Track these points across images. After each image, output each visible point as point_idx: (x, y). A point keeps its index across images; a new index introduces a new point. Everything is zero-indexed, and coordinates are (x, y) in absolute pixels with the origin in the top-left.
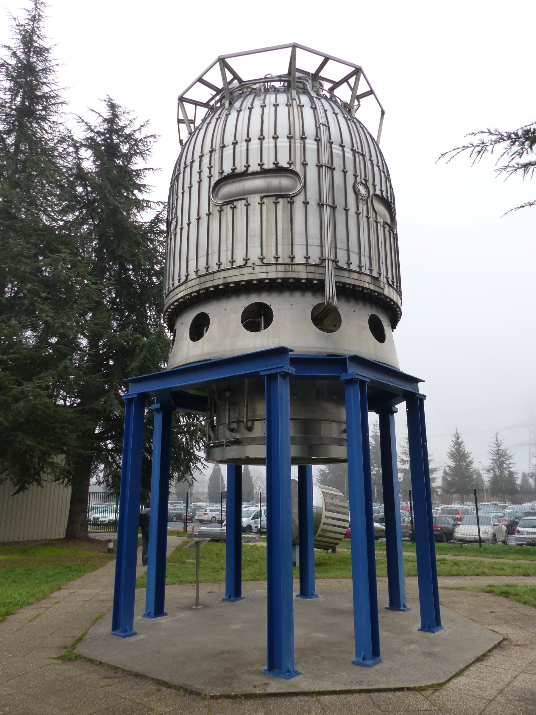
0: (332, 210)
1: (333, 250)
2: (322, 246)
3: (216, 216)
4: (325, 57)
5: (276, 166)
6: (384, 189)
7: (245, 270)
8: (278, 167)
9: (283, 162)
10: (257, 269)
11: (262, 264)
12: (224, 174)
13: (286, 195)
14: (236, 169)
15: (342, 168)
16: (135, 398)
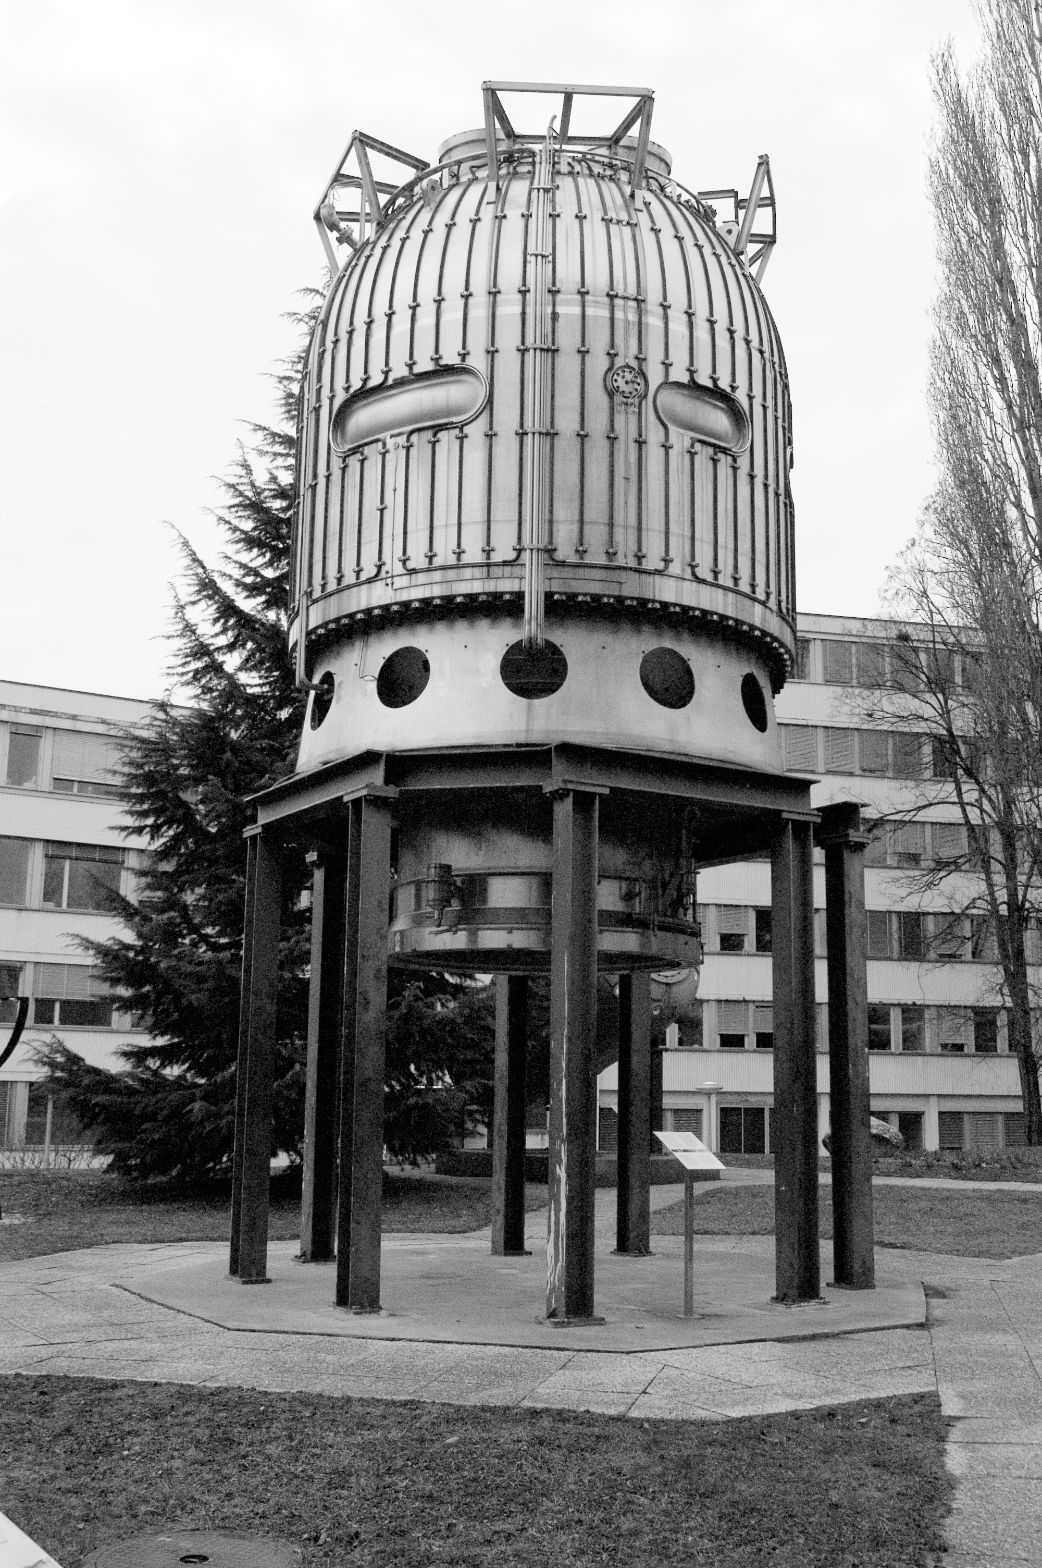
5: (437, 364)
7: (379, 586)
9: (450, 357)
10: (399, 582)
12: (352, 391)
13: (452, 423)
15: (684, 306)
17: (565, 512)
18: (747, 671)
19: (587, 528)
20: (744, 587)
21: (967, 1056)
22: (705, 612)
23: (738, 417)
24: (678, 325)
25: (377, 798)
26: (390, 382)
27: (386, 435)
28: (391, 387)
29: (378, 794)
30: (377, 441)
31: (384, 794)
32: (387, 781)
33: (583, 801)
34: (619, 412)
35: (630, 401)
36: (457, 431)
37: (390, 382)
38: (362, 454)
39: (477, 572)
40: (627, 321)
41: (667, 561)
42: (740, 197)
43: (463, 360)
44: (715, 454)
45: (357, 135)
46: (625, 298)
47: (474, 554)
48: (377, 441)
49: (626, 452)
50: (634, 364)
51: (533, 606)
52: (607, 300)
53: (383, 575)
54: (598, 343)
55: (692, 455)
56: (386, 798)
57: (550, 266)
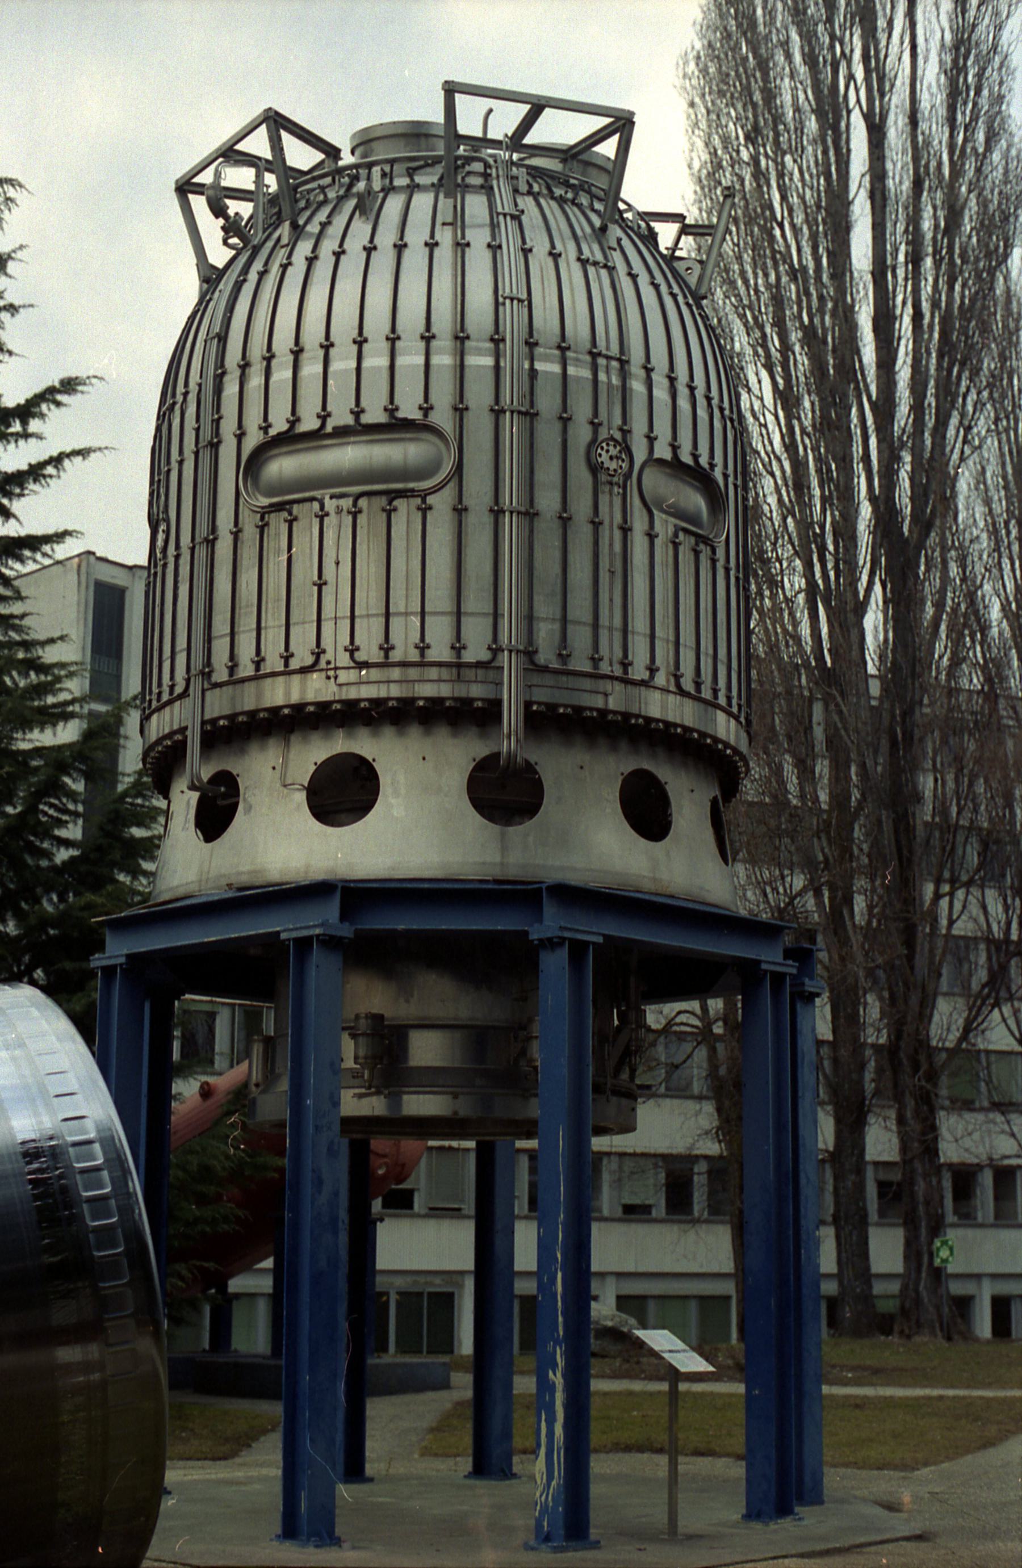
0: (525, 521)
1: (524, 624)
2: (496, 616)
3: (250, 532)
4: (533, 104)
6: (718, 459)
8: (396, 419)
9: (409, 409)
11: (352, 664)
12: (273, 432)
13: (413, 490)
14: (298, 420)
16: (121, 965)
17: (545, 608)
18: (629, 764)
19: (570, 628)
20: (706, 694)
21: (656, 1221)
22: (667, 724)
23: (716, 499)
24: (661, 393)
25: (332, 937)
26: (329, 429)
27: (325, 493)
28: (329, 436)
29: (333, 933)
30: (312, 499)
31: (339, 934)
32: (344, 917)
33: (578, 950)
34: (603, 492)
35: (615, 479)
36: (419, 501)
37: (329, 429)
38: (290, 514)
39: (445, 674)
40: (609, 383)
41: (652, 670)
42: (687, 221)
43: (426, 415)
44: (697, 544)
45: (272, 114)
46: (608, 358)
47: (440, 651)
48: (312, 499)
49: (611, 538)
50: (618, 436)
51: (511, 716)
52: (588, 358)
53: (323, 664)
54: (581, 409)
55: (676, 545)
56: (341, 938)
57: (526, 310)
